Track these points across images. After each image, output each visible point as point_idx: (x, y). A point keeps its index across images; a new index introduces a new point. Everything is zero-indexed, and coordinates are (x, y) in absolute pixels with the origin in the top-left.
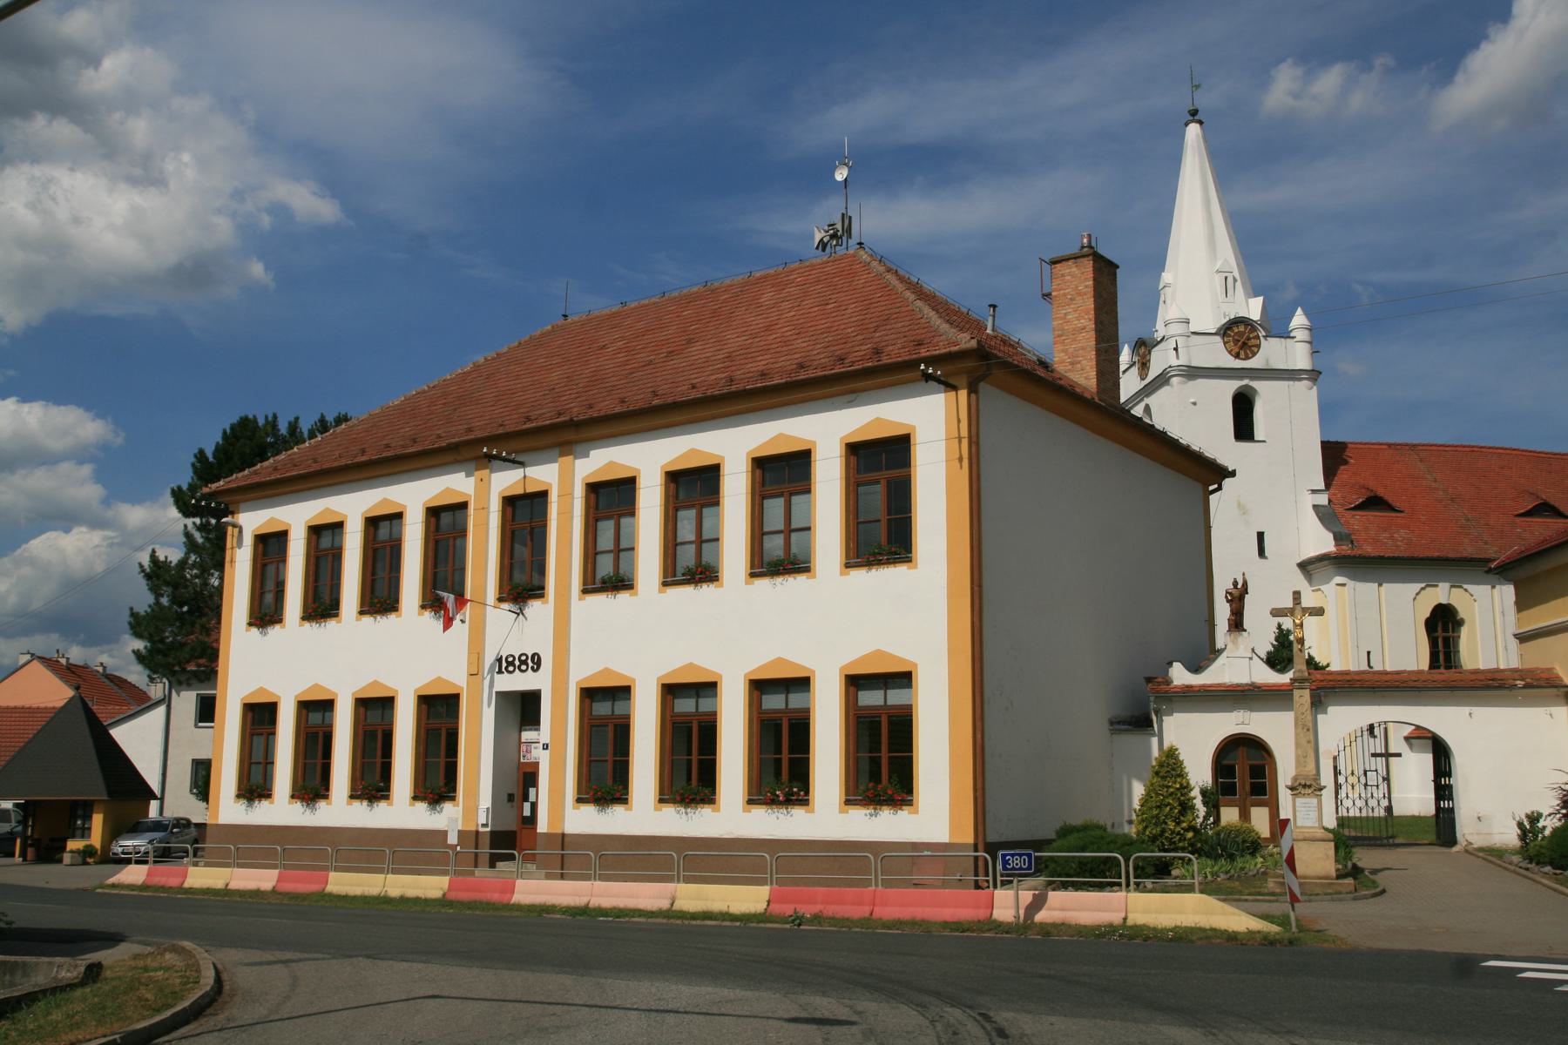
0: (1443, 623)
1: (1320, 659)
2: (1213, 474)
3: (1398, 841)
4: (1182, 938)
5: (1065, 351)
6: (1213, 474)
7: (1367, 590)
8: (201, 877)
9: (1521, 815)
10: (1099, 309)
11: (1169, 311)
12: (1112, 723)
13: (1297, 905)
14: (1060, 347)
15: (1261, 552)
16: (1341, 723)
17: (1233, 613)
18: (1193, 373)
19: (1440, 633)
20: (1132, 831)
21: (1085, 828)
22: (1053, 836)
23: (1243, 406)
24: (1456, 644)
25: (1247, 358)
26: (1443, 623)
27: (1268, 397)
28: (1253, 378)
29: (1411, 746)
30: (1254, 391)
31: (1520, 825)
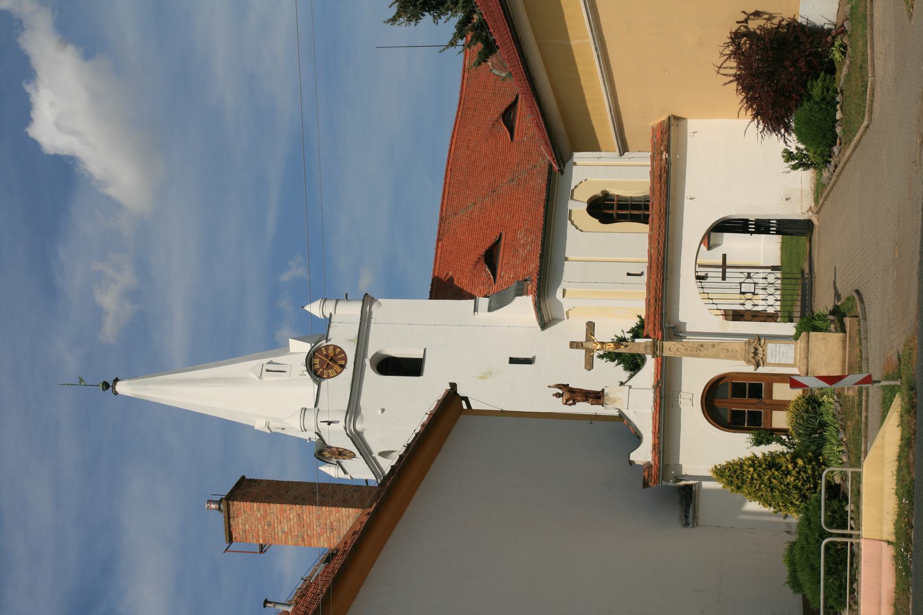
0: (605, 209)
1: (634, 322)
2: (451, 404)
3: (807, 271)
4: (911, 490)
5: (319, 535)
6: (451, 404)
7: (570, 272)
9: (786, 166)
10: (282, 500)
11: (293, 426)
12: (686, 524)
13: (874, 378)
14: (314, 541)
15: (529, 361)
16: (695, 310)
17: (586, 400)
18: (353, 409)
19: (614, 212)
20: (795, 518)
21: (792, 564)
22: (799, 597)
23: (391, 366)
24: (626, 199)
25: (345, 359)
26: (605, 209)
28: (365, 355)
29: (716, 245)
30: (376, 354)
31: (795, 167)
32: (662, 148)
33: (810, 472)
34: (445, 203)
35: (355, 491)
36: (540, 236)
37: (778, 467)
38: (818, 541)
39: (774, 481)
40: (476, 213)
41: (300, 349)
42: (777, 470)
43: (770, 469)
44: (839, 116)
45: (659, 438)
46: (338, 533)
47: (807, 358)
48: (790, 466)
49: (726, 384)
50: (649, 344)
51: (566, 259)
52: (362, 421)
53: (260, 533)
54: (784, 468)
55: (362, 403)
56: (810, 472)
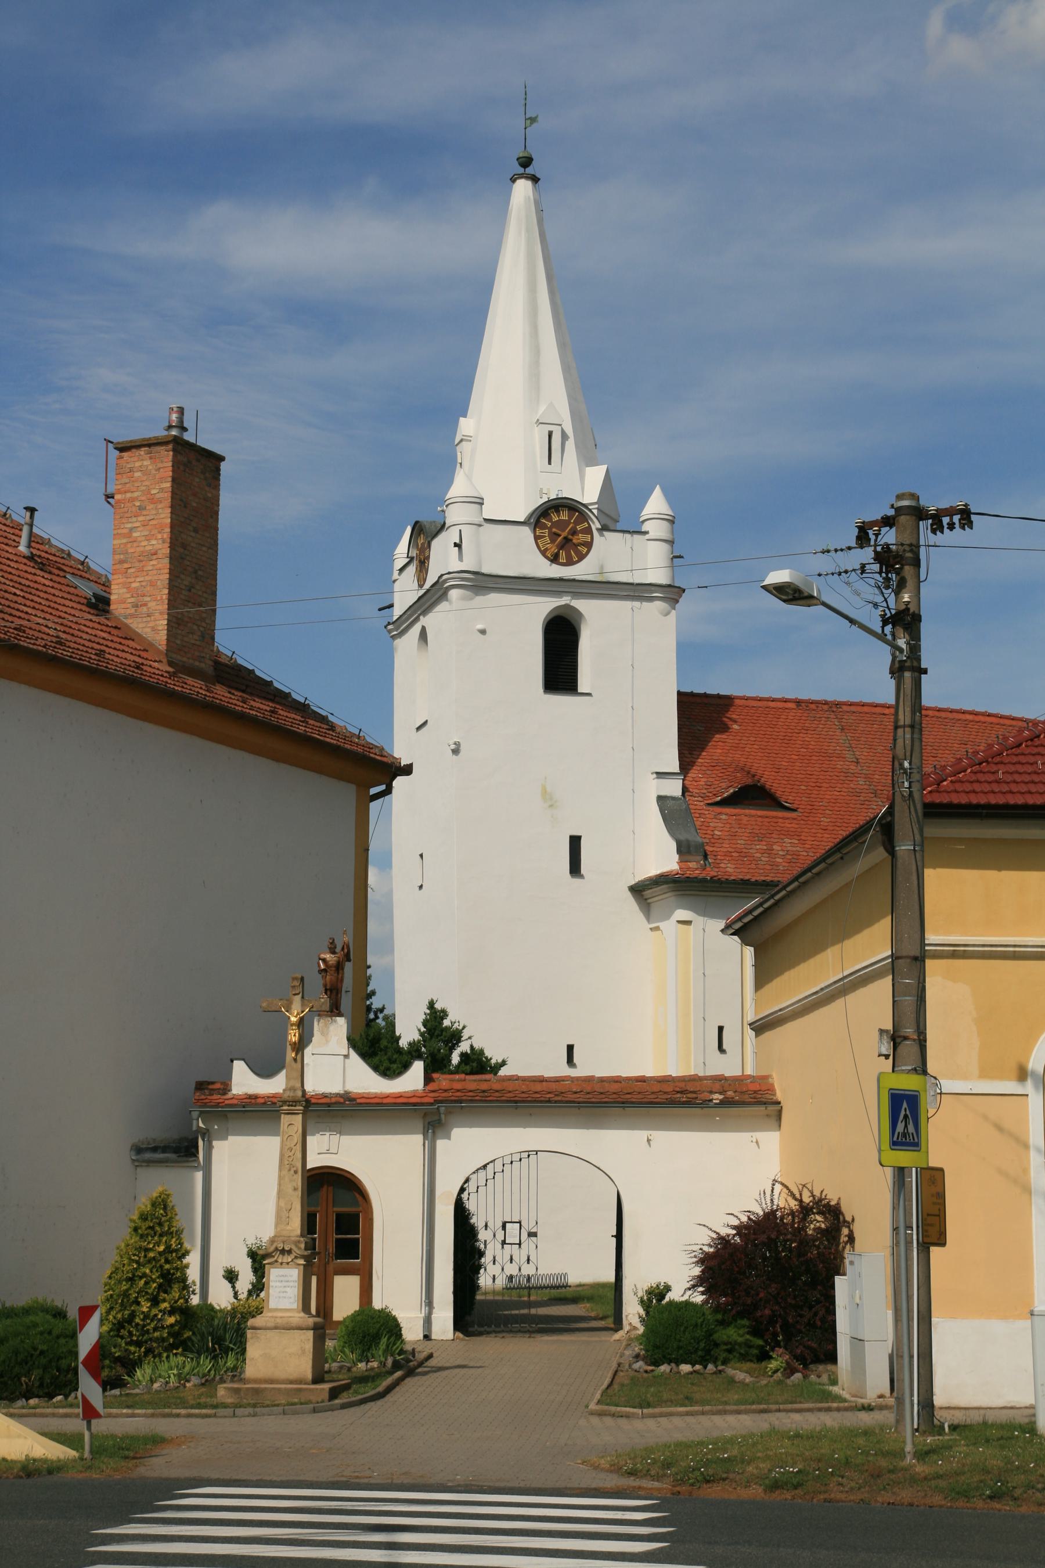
8: (533, 1311)
10: (177, 527)
12: (138, 1150)
13: (94, 1422)
15: (575, 868)
18: (481, 583)
23: (561, 645)
25: (570, 563)
27: (600, 625)
28: (577, 595)
30: (580, 615)
32: (730, 1093)
33: (157, 1334)
34: (866, 709)
35: (203, 636)
37: (166, 1285)
39: (142, 1282)
40: (840, 765)
41: (587, 487)
42: (160, 1286)
43: (162, 1276)
44: (686, 1368)
45: (265, 1103)
46: (132, 616)
47: (276, 1328)
48: (165, 1305)
52: (463, 598)
53: (129, 495)
54: (163, 1295)
55: (494, 598)
56: (157, 1334)
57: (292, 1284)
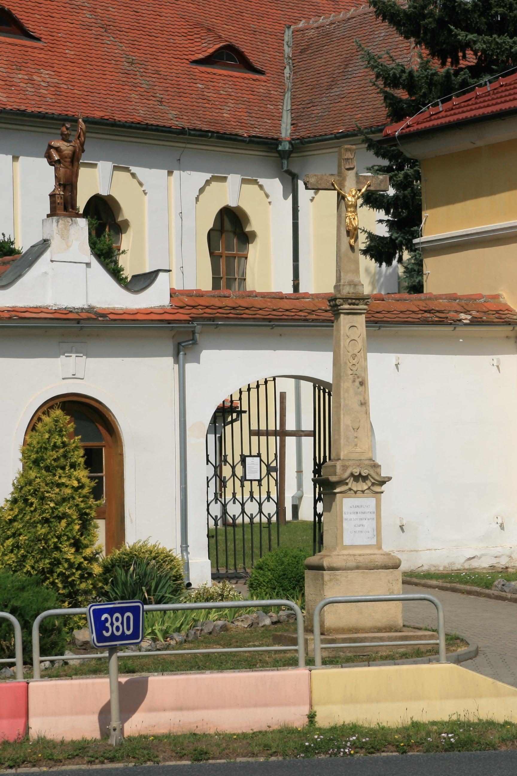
0: (231, 230)
26: (231, 230)
33: (83, 586)
36: (55, 111)
38: (6, 606)
45: (10, 318)
47: (358, 568)
49: (100, 437)
50: (359, 289)
51: (15, 158)
56: (83, 586)
57: (369, 516)
